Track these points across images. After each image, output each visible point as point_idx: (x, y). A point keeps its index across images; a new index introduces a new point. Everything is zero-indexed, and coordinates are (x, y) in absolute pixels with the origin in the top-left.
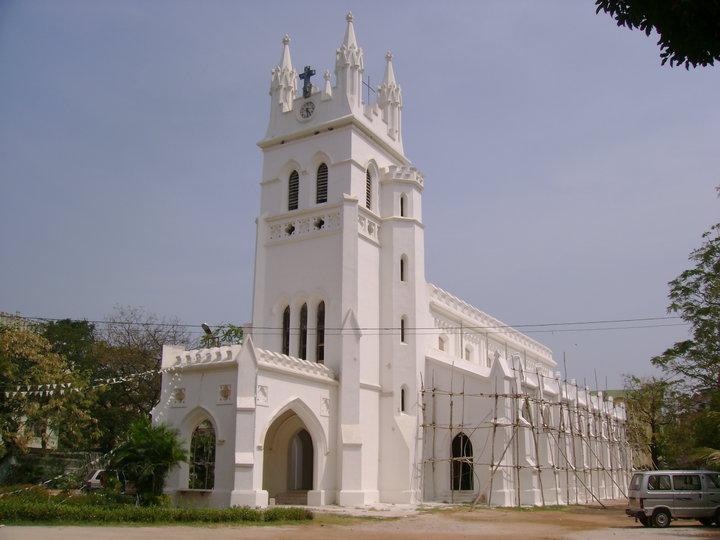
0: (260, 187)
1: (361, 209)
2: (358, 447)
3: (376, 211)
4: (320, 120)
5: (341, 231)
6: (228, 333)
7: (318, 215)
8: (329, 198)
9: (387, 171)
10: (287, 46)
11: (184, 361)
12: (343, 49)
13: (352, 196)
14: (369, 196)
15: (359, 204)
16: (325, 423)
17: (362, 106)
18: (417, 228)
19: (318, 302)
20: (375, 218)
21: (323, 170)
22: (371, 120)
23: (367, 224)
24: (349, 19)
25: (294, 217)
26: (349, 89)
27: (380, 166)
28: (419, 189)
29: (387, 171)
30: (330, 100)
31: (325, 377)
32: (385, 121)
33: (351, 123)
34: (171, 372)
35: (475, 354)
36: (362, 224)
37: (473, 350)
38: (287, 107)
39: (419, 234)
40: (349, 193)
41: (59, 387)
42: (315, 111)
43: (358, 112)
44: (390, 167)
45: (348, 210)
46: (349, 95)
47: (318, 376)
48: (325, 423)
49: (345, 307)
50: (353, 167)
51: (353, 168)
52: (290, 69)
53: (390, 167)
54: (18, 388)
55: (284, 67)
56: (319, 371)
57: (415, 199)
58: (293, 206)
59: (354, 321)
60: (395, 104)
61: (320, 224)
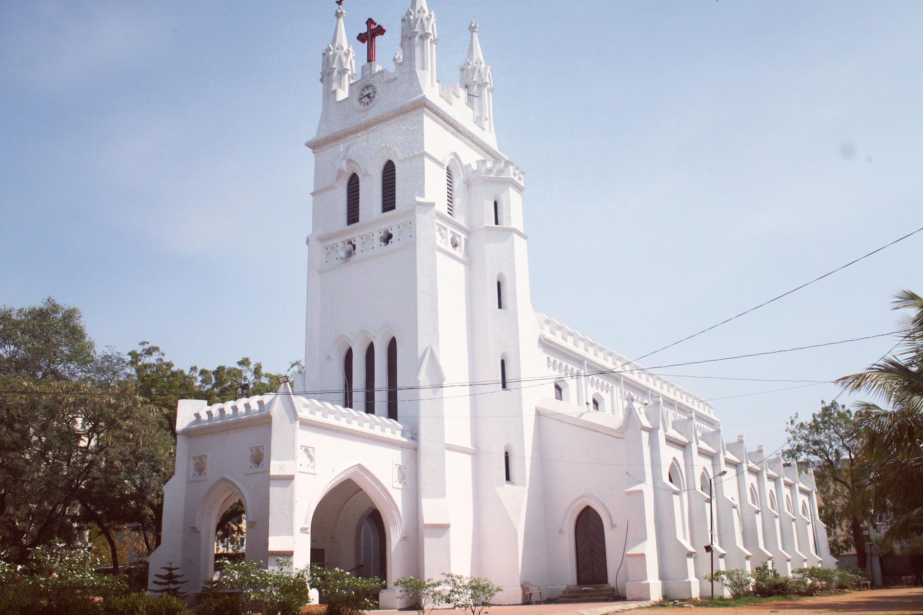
0: (311, 197)
1: (439, 216)
2: (445, 527)
3: (460, 219)
4: (385, 102)
5: (416, 249)
6: (397, 584)
7: (385, 226)
8: (397, 207)
9: (475, 167)
10: (341, 20)
11: (204, 417)
12: (409, 13)
13: (427, 199)
14: (450, 198)
15: (437, 207)
16: (398, 496)
17: (436, 85)
18: (516, 238)
19: (388, 340)
20: (460, 228)
21: (389, 171)
22: (451, 104)
23: (450, 236)
24: (472, 29)
25: (356, 233)
26: (418, 63)
27: (465, 162)
28: (519, 189)
29: (475, 167)
30: (396, 79)
31: (398, 436)
32: (470, 103)
33: (423, 105)
34: (187, 433)
35: (606, 404)
36: (442, 235)
37: (602, 399)
38: (342, 94)
39: (520, 245)
40: (423, 196)
41: (79, 559)
42: (377, 97)
43: (431, 91)
44: (478, 162)
45: (421, 218)
46: (419, 72)
47: (388, 434)
48: (398, 496)
49: (423, 343)
50: (426, 159)
51: (427, 161)
52: (345, 47)
53: (478, 162)
54: (6, 570)
55: (337, 45)
56: (391, 430)
57: (514, 204)
58: (353, 216)
59: (433, 358)
60: (482, 85)
61: (387, 238)
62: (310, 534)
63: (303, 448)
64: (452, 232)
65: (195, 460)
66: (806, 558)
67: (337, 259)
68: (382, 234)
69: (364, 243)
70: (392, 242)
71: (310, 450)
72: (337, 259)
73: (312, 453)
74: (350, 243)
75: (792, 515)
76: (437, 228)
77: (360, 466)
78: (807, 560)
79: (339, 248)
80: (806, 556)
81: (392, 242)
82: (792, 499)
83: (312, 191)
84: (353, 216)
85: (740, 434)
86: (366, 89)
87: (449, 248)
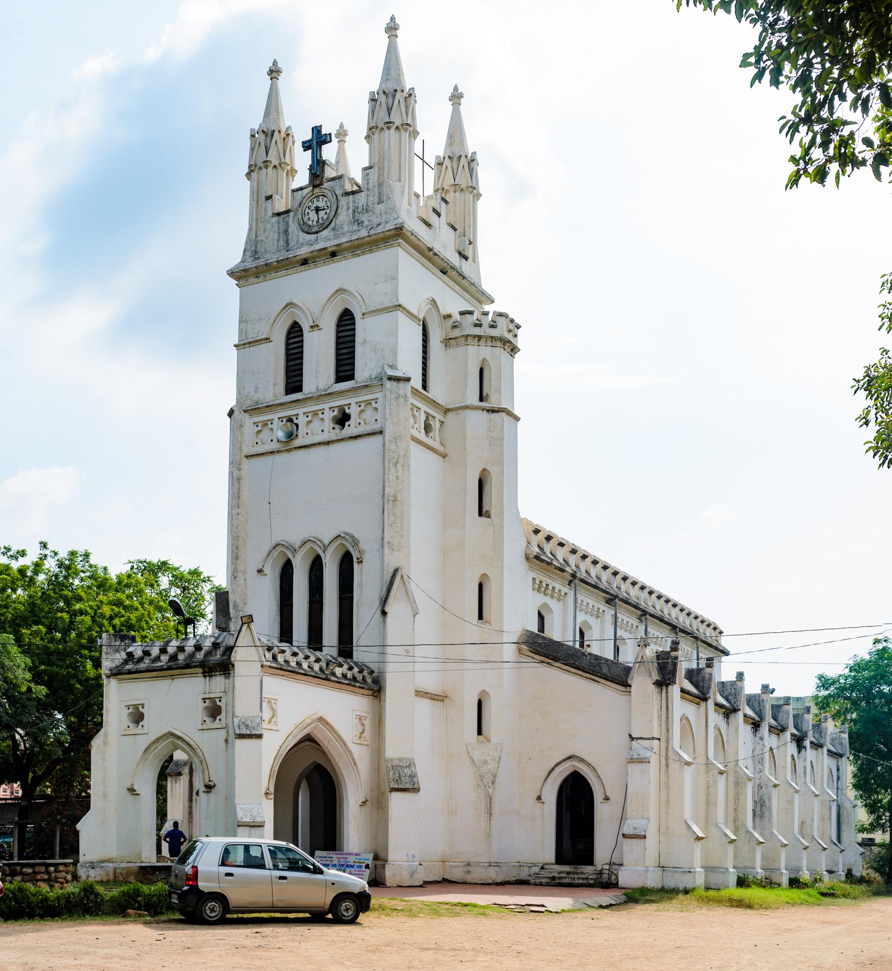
1: (414, 391)
62: (273, 801)
63: (358, 717)
64: (425, 412)
65: (129, 709)
66: (786, 842)
67: (272, 440)
68: (336, 413)
69: (310, 422)
70: (349, 425)
71: (273, 702)
72: (272, 440)
73: (274, 706)
74: (290, 420)
75: (772, 778)
76: (410, 406)
77: (321, 719)
78: (827, 849)
79: (275, 426)
80: (786, 839)
81: (349, 425)
82: (727, 735)
83: (236, 342)
84: (294, 382)
85: (741, 670)
86: (315, 200)
87: (422, 436)
